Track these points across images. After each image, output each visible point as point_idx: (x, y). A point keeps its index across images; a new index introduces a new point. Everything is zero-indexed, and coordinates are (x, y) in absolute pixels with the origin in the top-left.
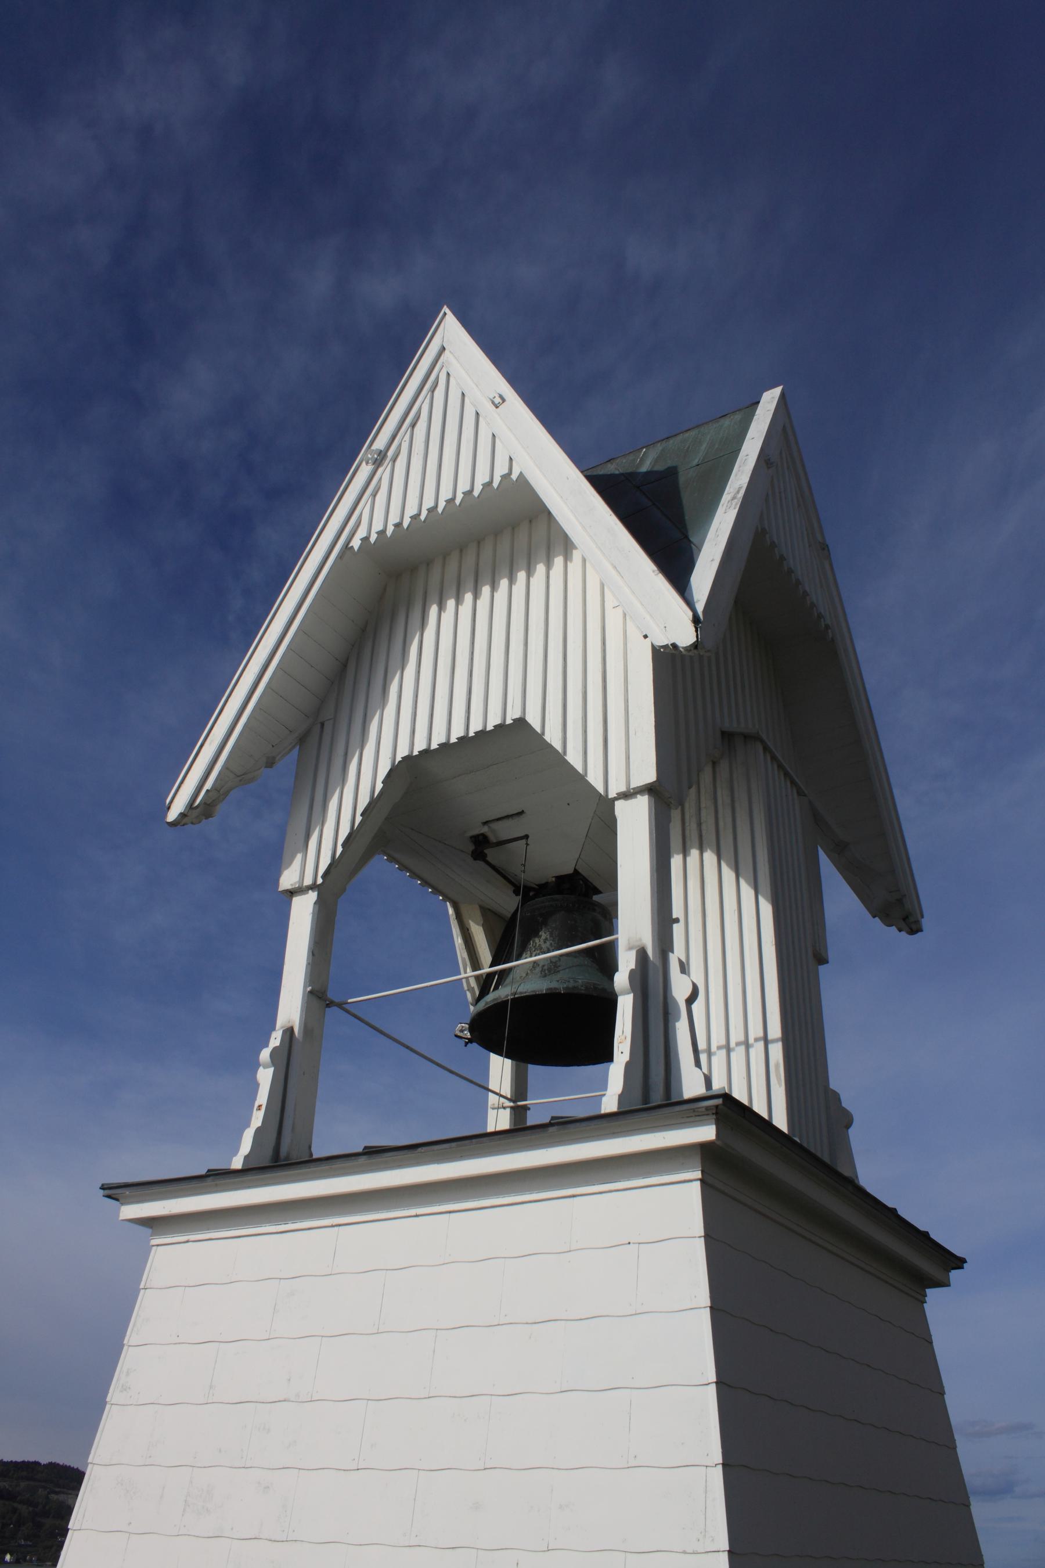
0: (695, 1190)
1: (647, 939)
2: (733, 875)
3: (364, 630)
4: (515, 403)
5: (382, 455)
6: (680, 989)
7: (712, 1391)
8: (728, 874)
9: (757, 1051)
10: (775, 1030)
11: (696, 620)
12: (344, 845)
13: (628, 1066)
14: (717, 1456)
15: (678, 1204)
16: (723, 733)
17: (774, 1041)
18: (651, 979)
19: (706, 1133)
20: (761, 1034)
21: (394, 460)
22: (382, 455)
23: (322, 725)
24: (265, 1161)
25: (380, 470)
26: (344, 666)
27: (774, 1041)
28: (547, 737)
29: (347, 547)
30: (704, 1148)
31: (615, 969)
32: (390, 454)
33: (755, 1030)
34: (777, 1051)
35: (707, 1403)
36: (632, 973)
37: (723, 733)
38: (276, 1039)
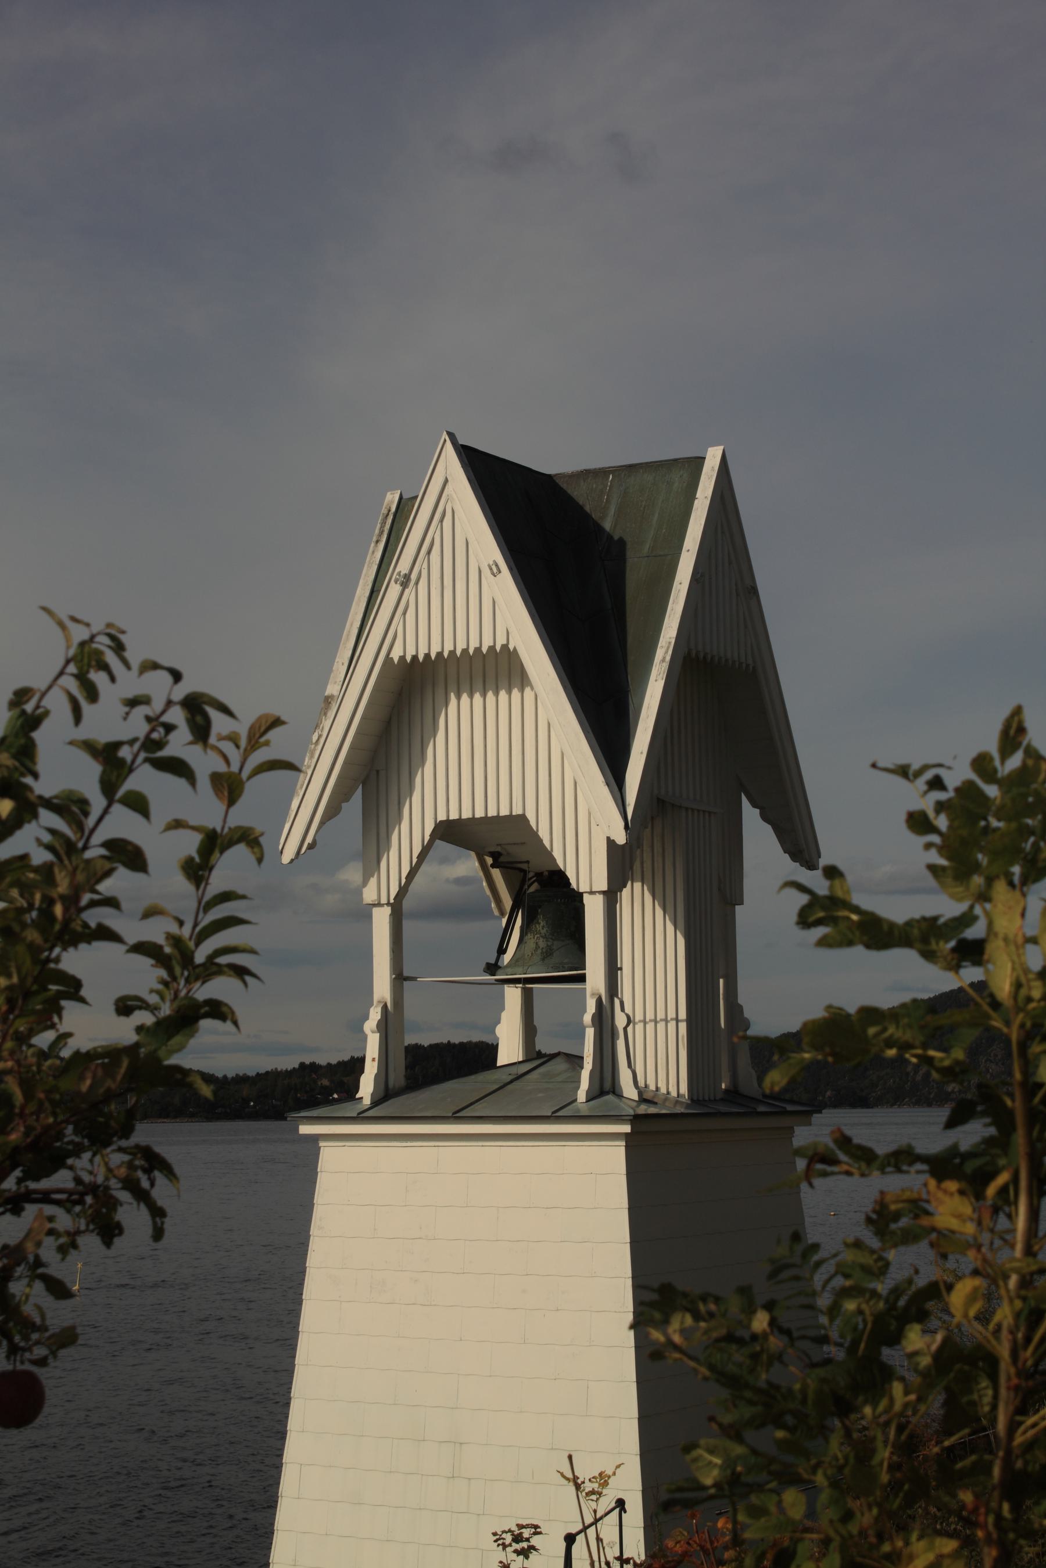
0: (623, 1149)
1: (602, 991)
2: (662, 912)
3: (400, 694)
4: (506, 575)
5: (407, 578)
6: (620, 1021)
7: (628, 1245)
8: (659, 912)
9: (672, 1025)
10: (683, 1014)
11: (626, 827)
12: (406, 878)
13: (591, 1072)
14: (630, 1275)
15: (613, 1158)
16: (658, 799)
17: (682, 1021)
18: (603, 1019)
19: (627, 1128)
20: (674, 1016)
21: (417, 583)
22: (407, 578)
23: (378, 772)
24: (381, 1094)
25: (407, 591)
26: (388, 723)
27: (682, 1021)
28: (540, 834)
29: (388, 659)
30: (627, 1134)
31: (585, 1011)
32: (414, 576)
33: (671, 1014)
34: (683, 1027)
35: (627, 1249)
36: (594, 1015)
37: (658, 799)
38: (375, 1015)
